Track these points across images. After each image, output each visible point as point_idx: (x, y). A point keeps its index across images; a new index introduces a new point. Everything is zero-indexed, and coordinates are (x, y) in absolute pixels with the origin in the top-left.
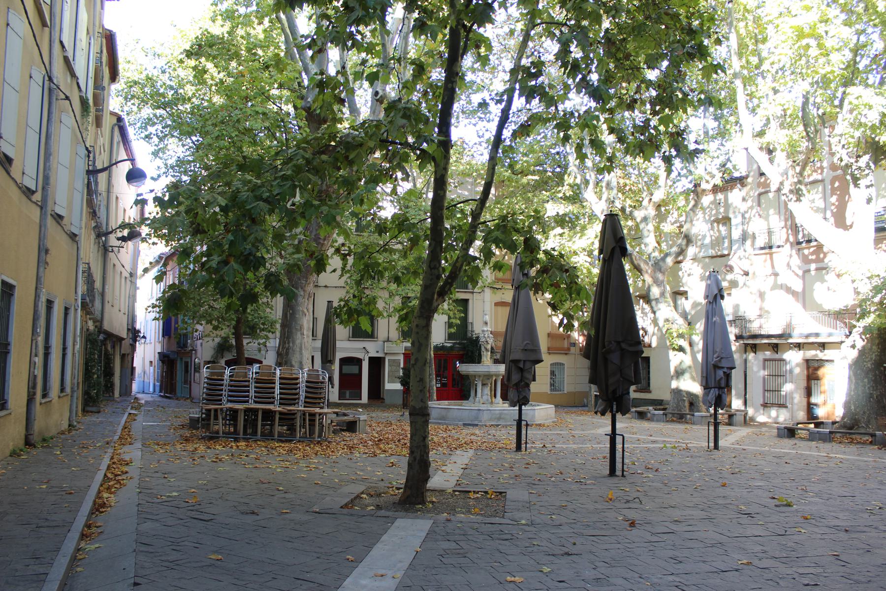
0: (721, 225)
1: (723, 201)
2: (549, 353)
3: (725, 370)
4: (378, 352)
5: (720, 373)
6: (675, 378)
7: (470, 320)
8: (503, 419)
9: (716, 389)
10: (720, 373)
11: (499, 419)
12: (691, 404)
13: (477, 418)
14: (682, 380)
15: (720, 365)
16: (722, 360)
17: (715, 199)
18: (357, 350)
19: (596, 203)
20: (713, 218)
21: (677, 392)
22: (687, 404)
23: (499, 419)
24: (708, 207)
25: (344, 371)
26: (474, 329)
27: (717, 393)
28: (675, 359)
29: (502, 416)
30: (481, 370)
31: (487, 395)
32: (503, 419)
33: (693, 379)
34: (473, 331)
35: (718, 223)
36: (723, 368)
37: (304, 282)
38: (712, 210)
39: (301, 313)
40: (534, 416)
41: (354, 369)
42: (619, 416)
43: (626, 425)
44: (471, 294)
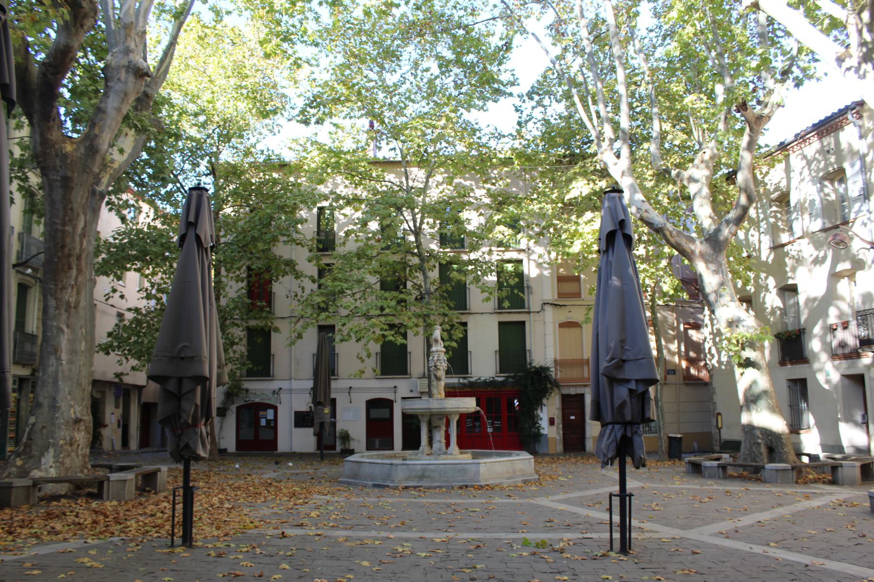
0: (836, 184)
1: (832, 146)
2: (687, 384)
3: (633, 386)
4: (412, 391)
5: (622, 392)
6: (744, 408)
7: (528, 347)
8: (428, 477)
9: (617, 427)
10: (622, 392)
11: (422, 477)
12: (771, 450)
13: (389, 477)
14: (754, 412)
15: (621, 376)
16: (627, 366)
17: (823, 147)
18: (388, 389)
19: (615, 164)
20: (821, 174)
21: (750, 429)
22: (763, 450)
23: (422, 477)
24: (815, 159)
25: (387, 411)
26: (533, 358)
27: (619, 435)
28: (745, 379)
29: (426, 474)
30: (415, 407)
31: (440, 442)
32: (428, 477)
33: (773, 409)
34: (531, 360)
35: (832, 181)
36: (628, 381)
37: (52, 286)
38: (819, 162)
39: (55, 331)
40: (477, 473)
41: (383, 413)
42: (630, 468)
43: (642, 484)
44: (527, 315)
